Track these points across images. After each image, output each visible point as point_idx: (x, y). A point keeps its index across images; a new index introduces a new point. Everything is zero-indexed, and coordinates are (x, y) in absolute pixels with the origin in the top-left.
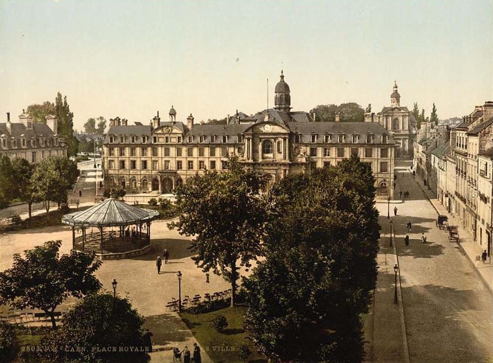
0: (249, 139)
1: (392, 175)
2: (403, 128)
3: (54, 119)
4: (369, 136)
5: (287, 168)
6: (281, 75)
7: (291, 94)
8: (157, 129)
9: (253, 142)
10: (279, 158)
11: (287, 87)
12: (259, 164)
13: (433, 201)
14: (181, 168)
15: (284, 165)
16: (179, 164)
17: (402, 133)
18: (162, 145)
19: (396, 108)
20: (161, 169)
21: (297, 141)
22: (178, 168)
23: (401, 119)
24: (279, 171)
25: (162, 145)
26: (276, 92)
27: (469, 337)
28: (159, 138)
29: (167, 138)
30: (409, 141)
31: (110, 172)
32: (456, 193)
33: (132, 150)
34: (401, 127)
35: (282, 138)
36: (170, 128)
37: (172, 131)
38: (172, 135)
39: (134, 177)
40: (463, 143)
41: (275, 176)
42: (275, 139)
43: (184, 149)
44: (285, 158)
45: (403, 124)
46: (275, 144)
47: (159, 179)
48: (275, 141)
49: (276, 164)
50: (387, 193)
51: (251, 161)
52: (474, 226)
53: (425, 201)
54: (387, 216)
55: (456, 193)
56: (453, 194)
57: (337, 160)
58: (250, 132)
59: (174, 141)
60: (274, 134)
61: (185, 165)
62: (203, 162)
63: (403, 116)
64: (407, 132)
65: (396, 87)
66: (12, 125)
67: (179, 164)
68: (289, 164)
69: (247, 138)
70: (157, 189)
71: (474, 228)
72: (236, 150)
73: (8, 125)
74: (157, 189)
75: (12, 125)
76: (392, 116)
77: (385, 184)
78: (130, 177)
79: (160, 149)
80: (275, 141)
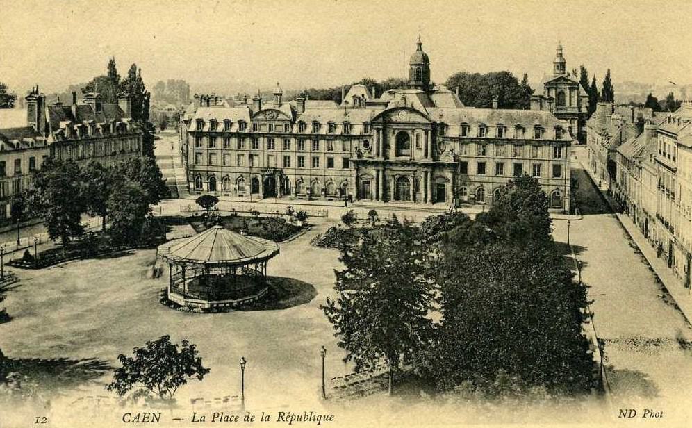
0: (378, 131)
1: (568, 182)
2: (570, 105)
3: (128, 98)
4: (537, 128)
5: (429, 170)
6: (417, 41)
7: (430, 67)
8: (258, 114)
9: (383, 133)
10: (419, 156)
11: (426, 59)
12: (391, 164)
13: (623, 217)
14: (289, 166)
15: (426, 165)
16: (286, 161)
17: (569, 111)
18: (264, 135)
19: (562, 78)
20: (262, 166)
21: (442, 133)
22: (285, 166)
23: (567, 92)
24: (417, 174)
25: (264, 135)
26: (411, 65)
27: (482, 398)
28: (260, 125)
29: (271, 126)
30: (578, 121)
31: (198, 168)
32: (658, 216)
33: (226, 140)
34: (567, 104)
35: (423, 130)
36: (275, 114)
37: (277, 117)
38: (277, 123)
39: (228, 175)
40: (669, 151)
41: (412, 180)
42: (413, 131)
43: (293, 141)
44: (426, 155)
45: (570, 101)
46: (413, 138)
47: (260, 178)
48: (413, 132)
49: (414, 164)
50: (561, 205)
51: (381, 159)
52: (686, 267)
53: (606, 217)
54: (567, 242)
55: (658, 216)
56: (654, 216)
57: (496, 160)
58: (380, 120)
59: (280, 129)
60: (414, 124)
61: (293, 161)
62: (318, 159)
63: (570, 88)
64: (576, 111)
65: (561, 49)
66: (78, 108)
67: (286, 161)
68: (431, 165)
69: (376, 129)
70: (257, 191)
71: (686, 270)
72: (362, 144)
73: (73, 109)
74: (257, 191)
75: (78, 108)
76: (556, 89)
77: (558, 193)
78: (223, 176)
79: (261, 139)
80: (413, 132)
